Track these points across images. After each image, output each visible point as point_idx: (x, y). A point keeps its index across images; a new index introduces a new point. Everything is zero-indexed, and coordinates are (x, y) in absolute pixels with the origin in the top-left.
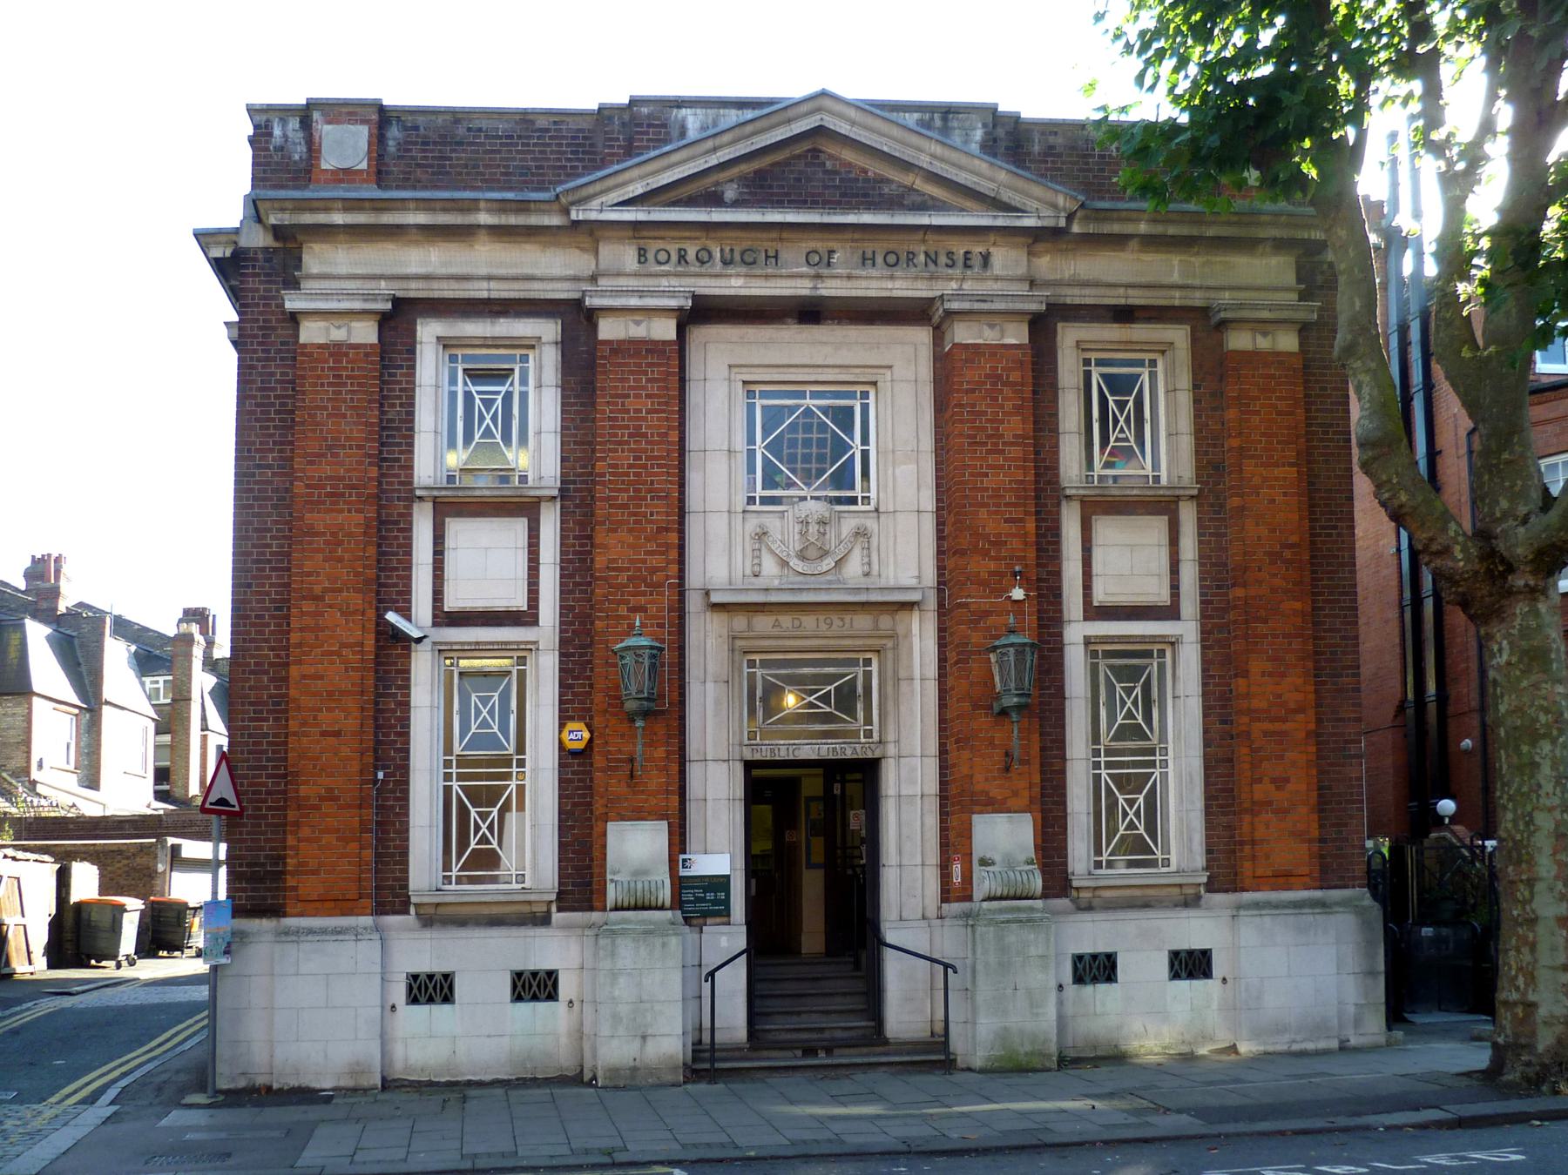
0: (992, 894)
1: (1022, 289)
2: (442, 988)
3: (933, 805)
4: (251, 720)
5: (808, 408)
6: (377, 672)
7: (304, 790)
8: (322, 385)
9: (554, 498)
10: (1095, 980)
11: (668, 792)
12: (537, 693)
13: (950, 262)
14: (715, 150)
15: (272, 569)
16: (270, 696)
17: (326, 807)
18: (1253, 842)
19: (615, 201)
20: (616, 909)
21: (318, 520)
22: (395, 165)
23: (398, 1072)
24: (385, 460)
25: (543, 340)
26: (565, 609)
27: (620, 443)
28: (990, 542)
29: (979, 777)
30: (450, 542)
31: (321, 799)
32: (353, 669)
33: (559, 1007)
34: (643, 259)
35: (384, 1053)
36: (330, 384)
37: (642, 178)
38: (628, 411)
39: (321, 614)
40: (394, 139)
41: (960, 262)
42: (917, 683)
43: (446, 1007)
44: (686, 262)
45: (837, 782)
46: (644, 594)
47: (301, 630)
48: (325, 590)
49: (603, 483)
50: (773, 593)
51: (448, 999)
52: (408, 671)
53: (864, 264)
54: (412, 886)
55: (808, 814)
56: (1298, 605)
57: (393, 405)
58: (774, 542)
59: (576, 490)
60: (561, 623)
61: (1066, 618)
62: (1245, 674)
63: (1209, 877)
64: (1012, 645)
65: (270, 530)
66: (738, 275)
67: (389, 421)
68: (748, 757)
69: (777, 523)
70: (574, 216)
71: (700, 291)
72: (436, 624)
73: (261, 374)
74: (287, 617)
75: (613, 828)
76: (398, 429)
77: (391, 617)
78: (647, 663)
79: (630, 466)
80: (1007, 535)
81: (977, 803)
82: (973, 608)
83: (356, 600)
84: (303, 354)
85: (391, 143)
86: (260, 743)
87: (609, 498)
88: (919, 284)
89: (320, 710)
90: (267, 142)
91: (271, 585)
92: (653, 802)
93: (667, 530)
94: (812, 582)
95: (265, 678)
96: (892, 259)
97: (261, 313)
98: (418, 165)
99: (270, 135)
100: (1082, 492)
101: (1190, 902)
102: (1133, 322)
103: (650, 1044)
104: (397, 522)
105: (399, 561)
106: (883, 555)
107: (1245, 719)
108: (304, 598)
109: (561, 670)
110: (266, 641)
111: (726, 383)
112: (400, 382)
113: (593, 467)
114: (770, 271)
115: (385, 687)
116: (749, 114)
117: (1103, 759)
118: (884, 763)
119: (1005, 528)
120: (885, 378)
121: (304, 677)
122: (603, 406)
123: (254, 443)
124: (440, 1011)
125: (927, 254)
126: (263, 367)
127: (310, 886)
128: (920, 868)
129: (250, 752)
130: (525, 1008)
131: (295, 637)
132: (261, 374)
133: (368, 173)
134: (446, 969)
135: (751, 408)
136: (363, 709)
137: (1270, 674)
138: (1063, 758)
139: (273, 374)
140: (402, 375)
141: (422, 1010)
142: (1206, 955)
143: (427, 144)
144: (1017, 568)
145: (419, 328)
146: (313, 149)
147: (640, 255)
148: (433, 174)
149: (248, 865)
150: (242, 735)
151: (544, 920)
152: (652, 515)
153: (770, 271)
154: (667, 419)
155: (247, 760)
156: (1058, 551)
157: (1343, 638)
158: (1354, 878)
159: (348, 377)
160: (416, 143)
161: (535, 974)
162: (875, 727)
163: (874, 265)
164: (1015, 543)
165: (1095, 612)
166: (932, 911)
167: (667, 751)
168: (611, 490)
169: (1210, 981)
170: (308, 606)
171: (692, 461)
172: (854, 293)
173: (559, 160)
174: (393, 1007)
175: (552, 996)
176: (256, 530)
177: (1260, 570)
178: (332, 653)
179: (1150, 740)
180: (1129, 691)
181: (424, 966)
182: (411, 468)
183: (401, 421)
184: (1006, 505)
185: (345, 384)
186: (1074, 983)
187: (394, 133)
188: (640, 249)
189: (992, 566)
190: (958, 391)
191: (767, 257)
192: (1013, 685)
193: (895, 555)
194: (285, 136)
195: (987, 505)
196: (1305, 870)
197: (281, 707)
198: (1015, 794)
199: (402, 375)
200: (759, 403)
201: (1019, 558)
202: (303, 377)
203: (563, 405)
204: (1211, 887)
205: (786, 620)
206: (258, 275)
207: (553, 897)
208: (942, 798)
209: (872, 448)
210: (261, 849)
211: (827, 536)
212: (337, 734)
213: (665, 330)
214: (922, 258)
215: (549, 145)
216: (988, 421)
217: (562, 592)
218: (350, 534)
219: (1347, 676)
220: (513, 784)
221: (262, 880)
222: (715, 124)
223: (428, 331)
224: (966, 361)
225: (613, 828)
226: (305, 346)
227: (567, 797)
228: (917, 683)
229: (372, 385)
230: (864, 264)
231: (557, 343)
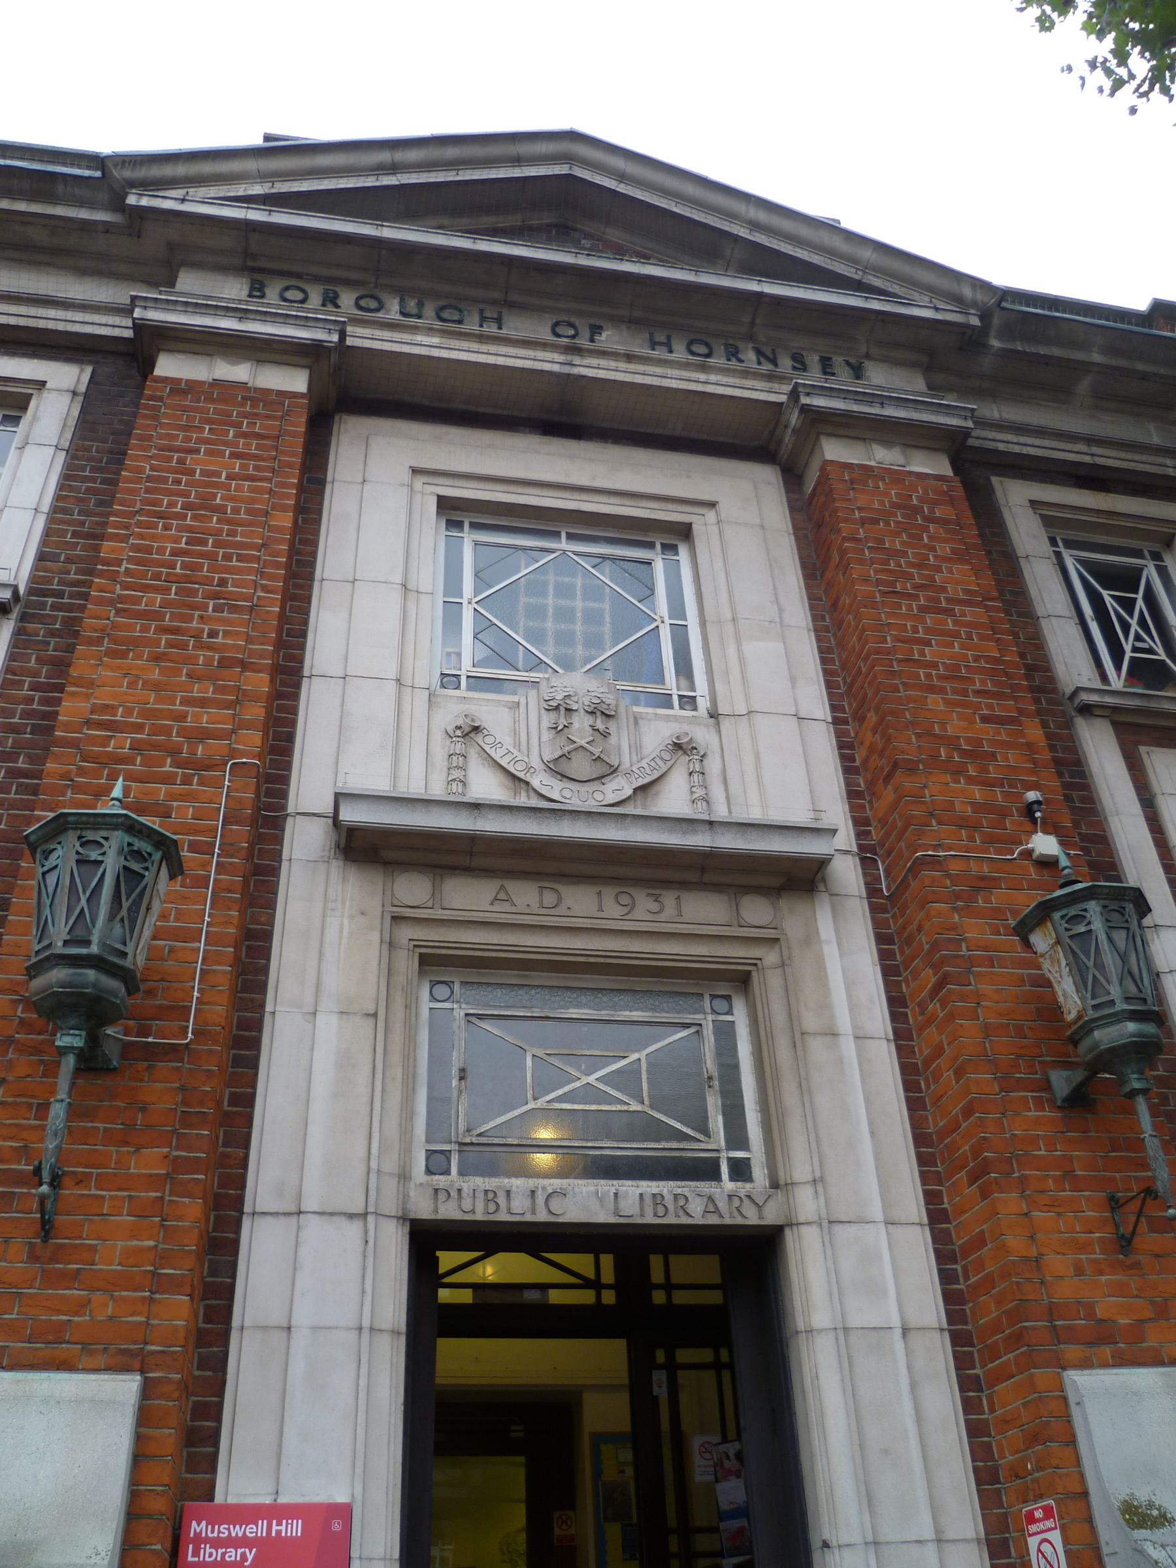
11: (158, 1283)
25: (48, 386)
27: (161, 516)
29: (1057, 1264)
42: (848, 1047)
45: (660, 1367)
46: (168, 779)
50: (492, 815)
55: (597, 1473)
68: (424, 1209)
78: (112, 863)
80: (992, 742)
92: (105, 1308)
93: (245, 666)
106: (735, 788)
118: (789, 1235)
119: (987, 732)
120: (703, 525)
147: (252, 289)
152: (213, 634)
162: (756, 1153)
164: (1013, 757)
168: (126, 586)
192: (1115, 992)
193: (760, 784)
208: (958, 1339)
211: (613, 740)
228: (848, 1047)
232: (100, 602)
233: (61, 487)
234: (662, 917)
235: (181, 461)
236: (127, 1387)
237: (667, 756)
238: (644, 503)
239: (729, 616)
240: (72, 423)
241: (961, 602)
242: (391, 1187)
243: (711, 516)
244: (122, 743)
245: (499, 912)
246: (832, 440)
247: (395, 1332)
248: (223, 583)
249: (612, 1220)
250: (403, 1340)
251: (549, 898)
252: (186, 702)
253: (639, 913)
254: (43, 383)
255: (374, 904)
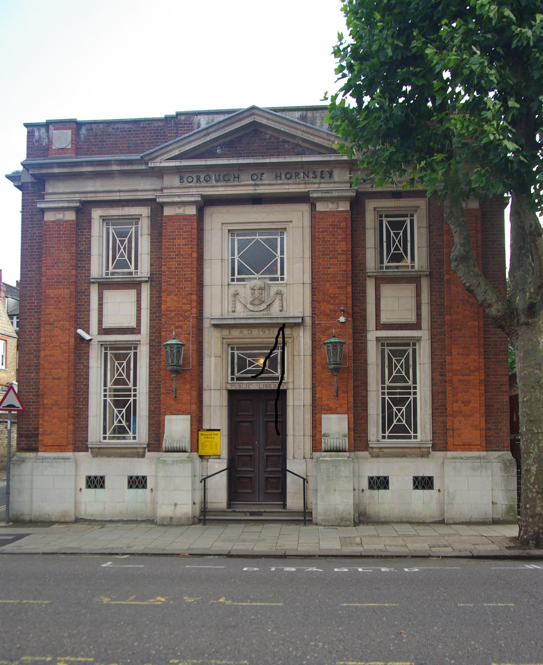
0: (167, 449)
1: (347, 186)
2: (100, 482)
3: (309, 410)
4: (27, 373)
5: (257, 239)
6: (75, 353)
7: (46, 401)
8: (53, 238)
9: (147, 281)
10: (379, 488)
12: (140, 362)
13: (314, 176)
14: (208, 134)
15: (35, 312)
16: (34, 363)
17: (55, 408)
18: (453, 430)
19: (167, 158)
20: (325, 451)
21: (51, 292)
22: (83, 145)
23: (82, 515)
24: (79, 267)
25: (143, 216)
26: (152, 327)
28: (330, 297)
29: (324, 399)
30: (105, 300)
31: (53, 405)
32: (65, 352)
33: (147, 491)
34: (199, 177)
35: (76, 507)
36: (56, 237)
37: (177, 148)
38: (175, 245)
39: (53, 330)
40: (83, 134)
41: (319, 176)
42: (302, 357)
43: (101, 490)
44: (200, 181)
46: (181, 321)
47: (45, 337)
48: (54, 321)
49: (165, 275)
51: (102, 487)
52: (89, 353)
53: (276, 179)
54: (89, 441)
56: (476, 323)
57: (82, 245)
58: (241, 297)
59: (157, 278)
60: (150, 333)
61: (368, 329)
62: (450, 354)
63: (432, 444)
64: (331, 343)
65: (34, 296)
66: (222, 186)
67: (81, 251)
68: (230, 388)
69: (243, 290)
70: (150, 165)
71: (203, 193)
72: (99, 334)
73: (30, 233)
74: (40, 332)
75: (167, 417)
76: (85, 254)
77: (80, 331)
79: (176, 268)
81: (324, 410)
82: (323, 325)
83: (67, 324)
84: (45, 225)
85: (82, 136)
86: (30, 382)
87: (167, 282)
88: (302, 186)
89: (52, 369)
90: (32, 138)
91: (35, 319)
93: (191, 294)
94: (257, 315)
95: (32, 356)
96: (288, 176)
97: (30, 209)
98: (93, 145)
99: (34, 135)
100: (375, 274)
101: (425, 455)
102: (401, 198)
103: (178, 507)
104: (84, 292)
105: (85, 308)
107: (451, 374)
108: (46, 324)
109: (150, 352)
110: (33, 341)
111: (220, 231)
112: (85, 235)
113: (161, 268)
114: (235, 183)
115: (79, 360)
116: (227, 116)
117: (386, 391)
118: (287, 390)
120: (289, 226)
121: (46, 356)
122: (165, 244)
123: (28, 261)
124: (99, 491)
125: (304, 173)
126: (31, 231)
127: (48, 440)
128: (302, 437)
129: (26, 386)
130: (133, 491)
131: (42, 340)
132: (30, 233)
133: (72, 150)
134: (101, 474)
135: (233, 241)
136: (69, 368)
137: (462, 354)
138: (366, 390)
139: (35, 233)
140: (86, 232)
141: (92, 491)
142: (431, 478)
143: (96, 136)
144: (342, 308)
145: (92, 212)
146: (50, 142)
147: (180, 179)
148: (99, 148)
149: (25, 431)
150: (23, 379)
151: (143, 456)
152: (185, 288)
153: (235, 183)
154: (191, 248)
155: (25, 389)
156: (365, 300)
157: (500, 338)
158: (504, 447)
159: (63, 234)
160: (92, 136)
161: (137, 477)
163: (281, 179)
165: (380, 326)
166: (308, 455)
167: (191, 386)
169: (432, 491)
170: (48, 327)
171: (206, 264)
172: (272, 191)
173: (151, 139)
174: (81, 489)
175: (144, 487)
176: (29, 297)
177: (458, 307)
178: (57, 346)
179: (408, 383)
180: (399, 361)
181: (93, 473)
182: (90, 270)
183: (86, 251)
184: (338, 281)
185: (62, 237)
186: (369, 489)
187: (83, 131)
188: (180, 177)
189: (331, 307)
190: (317, 232)
191: (234, 177)
194: (40, 136)
195: (330, 281)
196: (478, 443)
197: (38, 367)
198: (341, 406)
199: (86, 232)
200: (236, 238)
201: (343, 304)
202: (46, 235)
203: (151, 242)
204: (435, 448)
205: (245, 331)
206: (29, 193)
207: (145, 446)
209: (285, 256)
210: (30, 425)
211: (263, 295)
212: (59, 379)
213: (71, 216)
214: (302, 175)
215: (146, 133)
216: (330, 245)
217: (150, 320)
218: (64, 298)
219: (502, 355)
220: (132, 399)
221: (31, 437)
222: (212, 121)
223: (96, 214)
224: (321, 219)
225: (167, 417)
226: (46, 222)
227: (153, 404)
229: (73, 237)
230: (276, 179)
231: (148, 217)
232: (164, 282)
233: (151, 246)
234: (270, 334)
235: (173, 242)
236: (189, 417)
237: (275, 296)
238: (275, 224)
239: (292, 256)
240: (149, 226)
241: (340, 254)
242: (224, 385)
243: (291, 224)
244: (173, 314)
245: (241, 335)
246: (319, 203)
247: (226, 406)
248: (185, 275)
249: (259, 389)
250: (227, 407)
251: (250, 332)
252: (183, 304)
253: (266, 334)
254: (141, 215)
255: (219, 336)
